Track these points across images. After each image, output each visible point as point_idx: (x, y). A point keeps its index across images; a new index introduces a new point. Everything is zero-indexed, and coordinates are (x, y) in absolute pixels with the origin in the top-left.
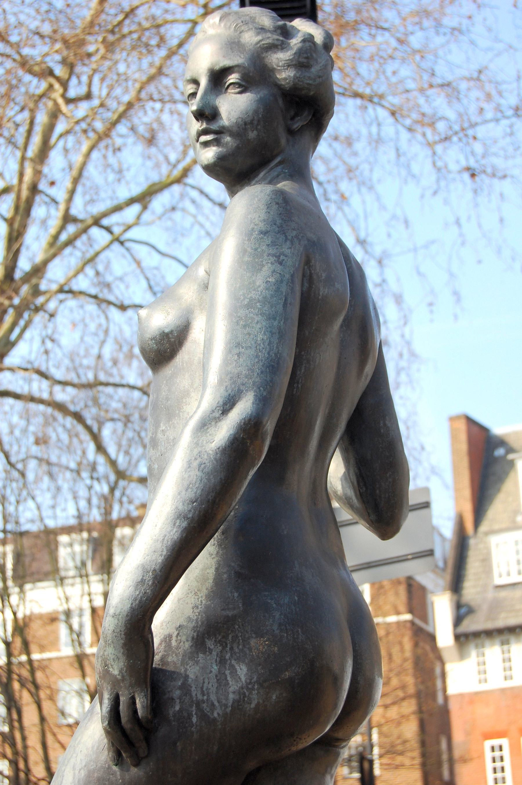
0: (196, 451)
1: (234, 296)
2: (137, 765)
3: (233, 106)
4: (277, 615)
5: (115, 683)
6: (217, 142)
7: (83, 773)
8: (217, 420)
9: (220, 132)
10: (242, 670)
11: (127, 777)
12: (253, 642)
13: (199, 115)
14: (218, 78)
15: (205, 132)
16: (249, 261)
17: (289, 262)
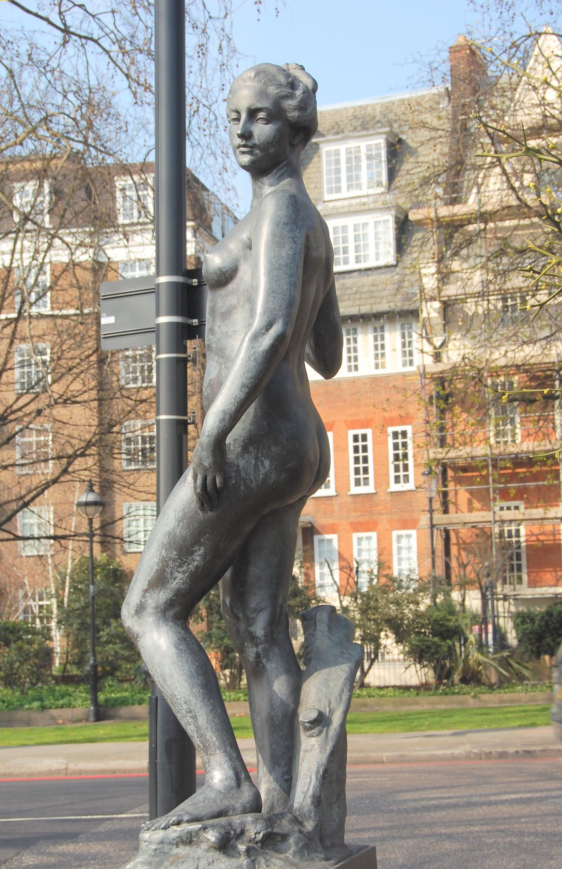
0: (252, 351)
1: (270, 262)
2: (211, 510)
3: (262, 131)
4: (285, 434)
5: (205, 469)
6: (250, 153)
7: (181, 514)
8: (264, 334)
9: (254, 147)
10: (267, 463)
11: (206, 516)
12: (273, 448)
13: (241, 136)
14: (252, 113)
15: (244, 146)
16: (277, 241)
17: (299, 242)
